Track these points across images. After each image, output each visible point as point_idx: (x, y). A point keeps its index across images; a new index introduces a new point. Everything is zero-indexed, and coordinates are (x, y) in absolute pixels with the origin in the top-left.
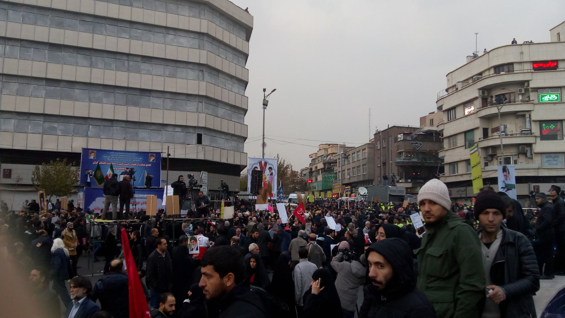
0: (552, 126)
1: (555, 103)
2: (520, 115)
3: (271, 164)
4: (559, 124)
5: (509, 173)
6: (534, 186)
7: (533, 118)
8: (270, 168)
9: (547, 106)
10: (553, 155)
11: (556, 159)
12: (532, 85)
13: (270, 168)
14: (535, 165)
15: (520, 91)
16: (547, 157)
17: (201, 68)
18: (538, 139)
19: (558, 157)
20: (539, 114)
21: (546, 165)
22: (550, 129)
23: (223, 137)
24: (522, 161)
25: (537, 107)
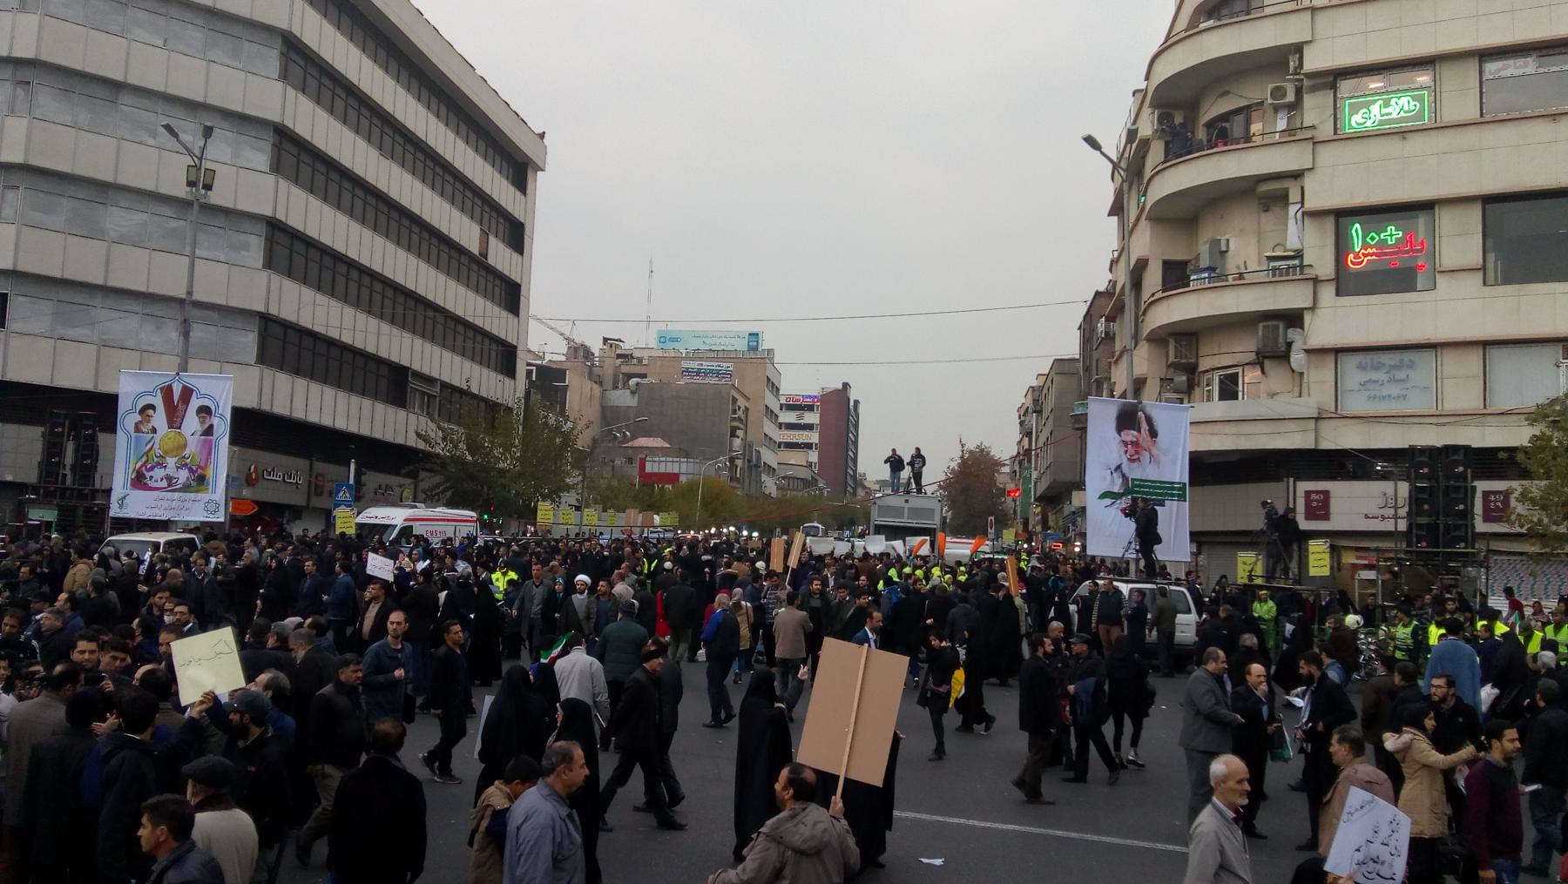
0: (1392, 234)
1: (1403, 134)
2: (1267, 194)
3: (204, 396)
4: (1422, 221)
5: (1153, 434)
6: (1308, 494)
7: (1311, 204)
8: (204, 411)
9: (1375, 148)
10: (1388, 359)
11: (1401, 375)
12: (1315, 61)
13: (204, 411)
14: (1307, 405)
15: (1278, 92)
16: (1362, 367)
17: (26, 74)
18: (1327, 293)
19: (1411, 366)
20: (1336, 181)
21: (1356, 403)
22: (1382, 243)
23: (723, 341)
24: (1276, 387)
25: (1327, 154)
